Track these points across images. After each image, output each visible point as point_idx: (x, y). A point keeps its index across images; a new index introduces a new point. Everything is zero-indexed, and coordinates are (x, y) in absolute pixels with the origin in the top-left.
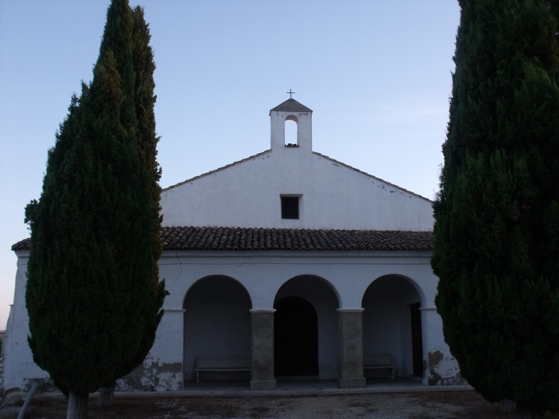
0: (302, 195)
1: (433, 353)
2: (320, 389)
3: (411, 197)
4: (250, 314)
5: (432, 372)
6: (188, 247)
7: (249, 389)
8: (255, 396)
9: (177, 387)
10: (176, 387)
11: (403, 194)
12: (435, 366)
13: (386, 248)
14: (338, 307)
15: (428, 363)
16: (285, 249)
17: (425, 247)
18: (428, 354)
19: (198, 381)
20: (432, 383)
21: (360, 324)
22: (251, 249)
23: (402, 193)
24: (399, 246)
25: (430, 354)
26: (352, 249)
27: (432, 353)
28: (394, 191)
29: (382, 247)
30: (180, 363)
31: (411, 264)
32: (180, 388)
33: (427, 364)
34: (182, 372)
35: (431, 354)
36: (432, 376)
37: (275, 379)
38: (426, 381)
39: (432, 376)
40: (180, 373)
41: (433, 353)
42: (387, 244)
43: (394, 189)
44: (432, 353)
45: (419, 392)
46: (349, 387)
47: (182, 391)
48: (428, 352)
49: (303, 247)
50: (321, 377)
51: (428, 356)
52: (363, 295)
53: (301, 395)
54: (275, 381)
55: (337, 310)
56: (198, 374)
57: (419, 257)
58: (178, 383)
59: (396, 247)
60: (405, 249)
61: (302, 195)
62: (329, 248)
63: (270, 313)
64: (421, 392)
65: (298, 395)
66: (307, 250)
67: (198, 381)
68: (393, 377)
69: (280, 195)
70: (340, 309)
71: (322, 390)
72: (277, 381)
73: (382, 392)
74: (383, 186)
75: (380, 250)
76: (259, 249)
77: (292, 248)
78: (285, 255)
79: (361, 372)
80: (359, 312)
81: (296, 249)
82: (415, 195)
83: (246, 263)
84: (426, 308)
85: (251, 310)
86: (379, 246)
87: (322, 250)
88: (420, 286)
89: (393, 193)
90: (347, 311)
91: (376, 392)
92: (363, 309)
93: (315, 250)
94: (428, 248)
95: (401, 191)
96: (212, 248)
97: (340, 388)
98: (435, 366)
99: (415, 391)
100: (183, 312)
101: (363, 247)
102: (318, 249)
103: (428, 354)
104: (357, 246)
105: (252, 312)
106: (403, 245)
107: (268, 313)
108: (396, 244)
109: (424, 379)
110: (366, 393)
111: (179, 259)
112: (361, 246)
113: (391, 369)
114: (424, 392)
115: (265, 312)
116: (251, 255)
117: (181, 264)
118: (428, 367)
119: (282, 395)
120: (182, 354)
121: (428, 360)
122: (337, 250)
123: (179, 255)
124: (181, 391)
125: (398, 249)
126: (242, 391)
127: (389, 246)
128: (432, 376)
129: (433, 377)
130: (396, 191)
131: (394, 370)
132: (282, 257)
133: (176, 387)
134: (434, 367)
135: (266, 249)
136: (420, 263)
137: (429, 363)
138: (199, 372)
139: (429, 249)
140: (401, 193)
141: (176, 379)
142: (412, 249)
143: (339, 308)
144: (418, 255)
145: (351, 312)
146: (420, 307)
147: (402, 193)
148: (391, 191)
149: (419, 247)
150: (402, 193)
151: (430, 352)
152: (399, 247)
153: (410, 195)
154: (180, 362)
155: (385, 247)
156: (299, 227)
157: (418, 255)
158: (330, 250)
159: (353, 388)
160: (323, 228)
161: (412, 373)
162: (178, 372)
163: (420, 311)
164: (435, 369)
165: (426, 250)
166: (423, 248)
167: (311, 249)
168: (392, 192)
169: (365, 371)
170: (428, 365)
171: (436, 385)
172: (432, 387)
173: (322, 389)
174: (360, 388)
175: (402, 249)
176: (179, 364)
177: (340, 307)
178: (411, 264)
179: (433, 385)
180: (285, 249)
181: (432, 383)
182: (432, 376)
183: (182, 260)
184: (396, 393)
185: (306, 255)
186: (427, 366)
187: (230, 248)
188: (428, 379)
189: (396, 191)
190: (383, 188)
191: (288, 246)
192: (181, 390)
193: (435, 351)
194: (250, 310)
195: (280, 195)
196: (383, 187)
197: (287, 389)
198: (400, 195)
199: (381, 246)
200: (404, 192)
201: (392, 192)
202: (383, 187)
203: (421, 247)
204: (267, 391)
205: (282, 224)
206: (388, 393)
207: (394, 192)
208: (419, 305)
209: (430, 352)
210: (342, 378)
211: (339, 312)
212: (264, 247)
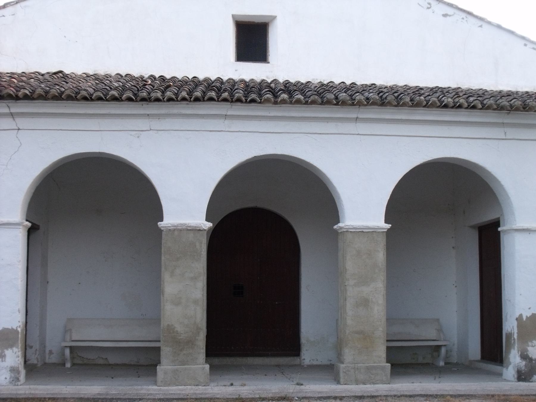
0: (274, 18)
1: (527, 317)
2: (298, 384)
3: (481, 26)
4: (160, 231)
5: (524, 356)
6: (30, 92)
7: (155, 383)
8: (162, 397)
9: (8, 378)
10: (6, 378)
11: (467, 21)
12: (530, 344)
13: (437, 102)
14: (337, 220)
15: (516, 336)
16: (230, 99)
17: (516, 103)
18: (517, 319)
19: (68, 365)
20: (522, 376)
21: (381, 256)
22: (161, 98)
23: (465, 18)
24: (464, 100)
25: (519, 319)
26: (368, 103)
27: (524, 318)
28: (449, 14)
29: (428, 102)
30: (15, 329)
31: (485, 139)
32: (15, 380)
33: (514, 339)
34: (17, 348)
35: (522, 319)
36: (524, 363)
37: (207, 362)
38: (510, 372)
39: (524, 363)
40: (15, 349)
41: (527, 317)
42: (438, 96)
43: (450, 11)
44: (524, 318)
45: (499, 395)
46: (357, 382)
47: (18, 385)
48: (517, 315)
49: (268, 95)
50: (304, 359)
51: (515, 324)
52: (388, 198)
53: (257, 396)
54: (207, 367)
55: (335, 227)
56: (67, 352)
57: (503, 125)
58: (10, 371)
59: (457, 102)
60: (474, 107)
61: (274, 18)
62: (320, 100)
63: (200, 230)
64: (504, 395)
65: (250, 396)
66: (276, 103)
67: (68, 365)
68: (442, 364)
69: (233, 16)
70: (340, 225)
71: (302, 387)
72: (210, 368)
73: (423, 393)
74: (429, 4)
75: (425, 106)
76: (177, 98)
77: (244, 99)
78: (230, 113)
79: (381, 352)
80: (379, 232)
81: (253, 101)
82: (489, 23)
83: (151, 130)
84: (514, 227)
85: (161, 224)
86: (422, 98)
87: (306, 103)
88: (503, 183)
89: (448, 17)
90: (354, 228)
91: (411, 394)
92: (389, 226)
93: (291, 103)
94: (521, 105)
95: (464, 15)
96: (80, 95)
97: (338, 382)
98: (530, 344)
99: (492, 393)
100: (21, 227)
101: (389, 98)
102: (298, 102)
103: (517, 319)
104: (377, 97)
105: (163, 227)
106: (471, 99)
107: (197, 230)
108: (456, 96)
109: (507, 368)
110: (391, 396)
111: (14, 120)
112: (386, 98)
113: (438, 347)
114: (511, 395)
115: (189, 228)
116: (163, 111)
117: (19, 129)
118: (516, 345)
119: (218, 396)
120: (19, 311)
121: (516, 331)
122: (337, 104)
123: (13, 110)
124: (15, 385)
125: (460, 106)
126: (139, 387)
127: (443, 99)
128: (524, 363)
129: (525, 366)
130: (453, 15)
131: (443, 350)
132: (226, 117)
133: (6, 378)
134: (529, 346)
135: (191, 98)
136: (504, 138)
137: (518, 336)
138: (71, 348)
139: (524, 108)
140: (463, 18)
141: (5, 361)
142: (489, 108)
143: (339, 223)
144: (500, 121)
145: (363, 232)
146: (499, 226)
147: (465, 18)
148: (444, 13)
149: (502, 104)
150: (465, 19)
151: (521, 315)
152: (462, 101)
153: (480, 23)
154: (15, 328)
155: (434, 102)
156: (267, 77)
157: (500, 121)
158: (322, 103)
159: (364, 384)
160: (313, 79)
161: (478, 356)
162: (11, 346)
163: (499, 233)
164: (530, 349)
165: (517, 109)
166: (511, 106)
167: (284, 102)
168: (445, 15)
169: (389, 349)
170: (516, 341)
171: (532, 382)
172: (523, 385)
173: (302, 385)
174: (378, 384)
175: (469, 106)
176: (14, 332)
177: (340, 222)
178: (485, 139)
179: (525, 380)
180: (230, 99)
181: (522, 376)
182: (524, 363)
183: (21, 122)
184: (451, 396)
185: (273, 114)
186: (514, 342)
187: (117, 95)
188: (516, 370)
189: (453, 15)
190: (428, 8)
191: (237, 95)
192: (16, 383)
193: (530, 314)
194: (159, 223)
195: (233, 16)
196: (429, 6)
197: (232, 385)
198: (462, 21)
199: (426, 98)
200: (468, 16)
201: (445, 15)
202: (429, 6)
203: (507, 104)
204: (189, 387)
205: (236, 70)
206: (437, 395)
207: (450, 16)
208: (497, 223)
209: (521, 315)
210: (343, 363)
211: (340, 231)
212: (186, 96)
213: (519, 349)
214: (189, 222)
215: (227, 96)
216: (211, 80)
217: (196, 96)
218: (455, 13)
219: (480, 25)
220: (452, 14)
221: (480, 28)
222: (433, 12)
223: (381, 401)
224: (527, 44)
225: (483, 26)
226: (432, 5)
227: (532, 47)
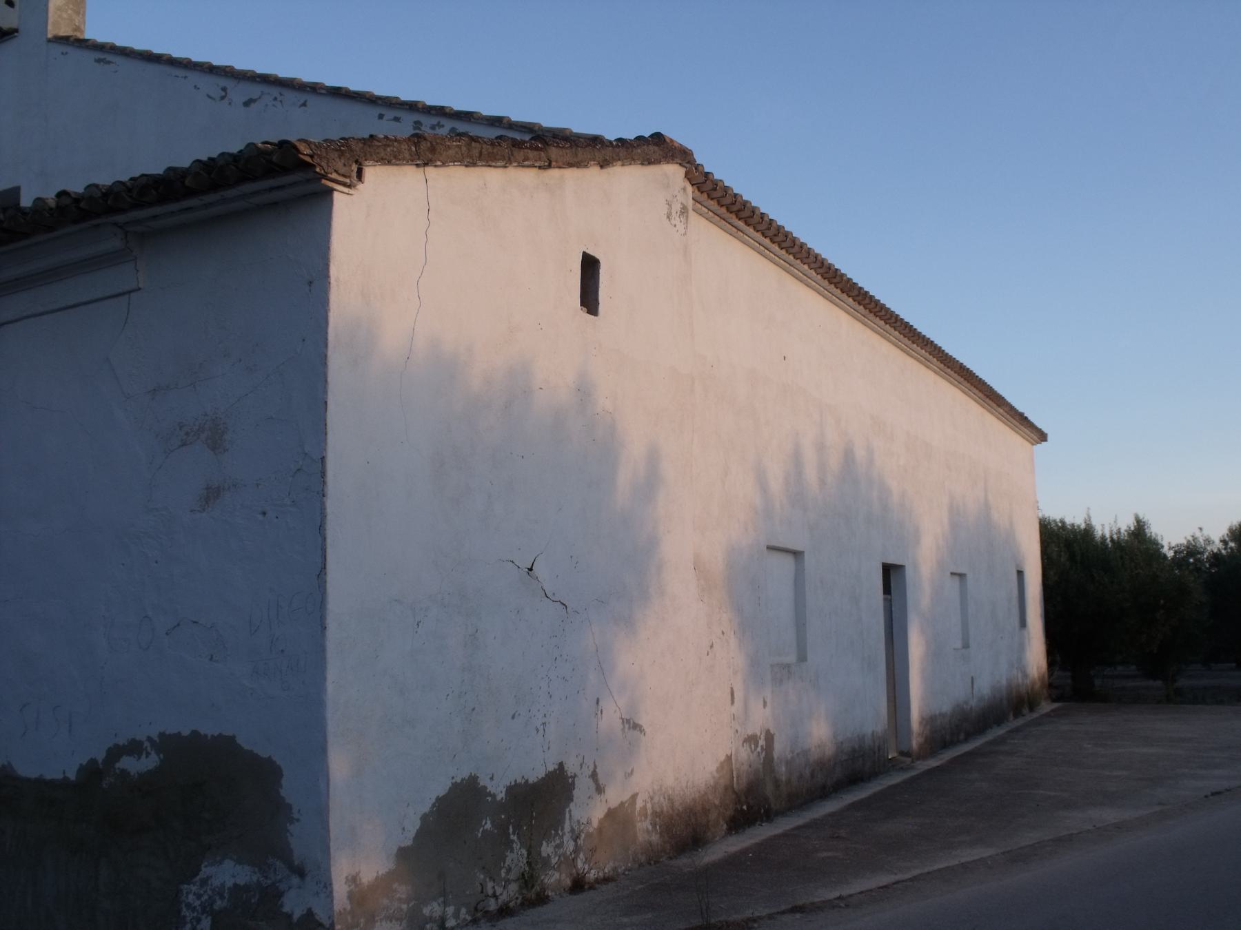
3: (304, 104)
11: (281, 101)
28: (254, 97)
130: (260, 98)
140: (275, 99)
189: (260, 98)
196: (223, 94)
201: (247, 104)
202: (223, 94)
213: (1185, 552)
214: (755, 233)
215: (639, 830)
216: (751, 204)
217: (656, 814)
218: (263, 93)
219: (302, 102)
220: (256, 97)
221: (303, 108)
222: (230, 103)
223: (656, 144)
224: (383, 113)
225: (308, 103)
226: (228, 91)
227: (392, 117)
